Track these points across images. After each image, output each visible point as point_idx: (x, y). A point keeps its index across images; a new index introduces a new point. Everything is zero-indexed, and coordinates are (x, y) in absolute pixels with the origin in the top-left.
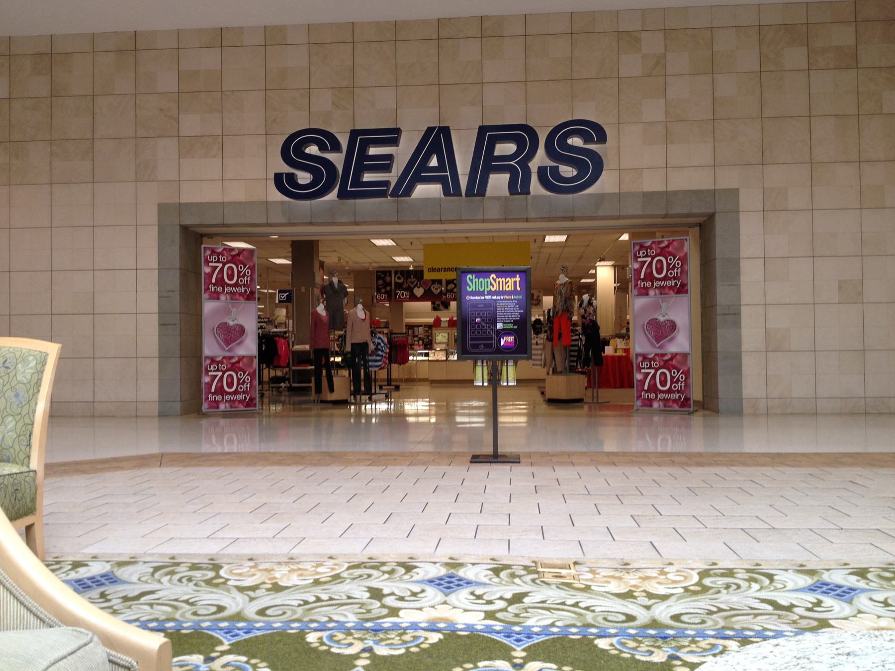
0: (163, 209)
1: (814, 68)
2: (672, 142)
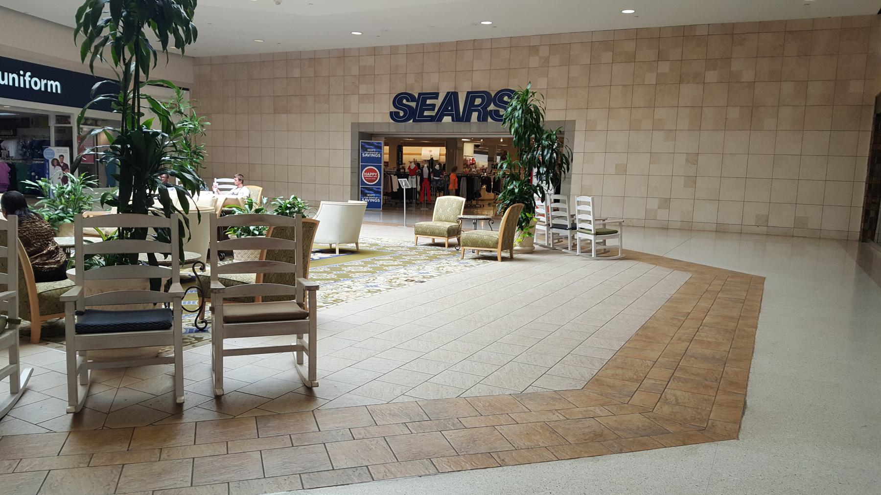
0: (353, 124)
1: (615, 62)
2: (549, 98)
